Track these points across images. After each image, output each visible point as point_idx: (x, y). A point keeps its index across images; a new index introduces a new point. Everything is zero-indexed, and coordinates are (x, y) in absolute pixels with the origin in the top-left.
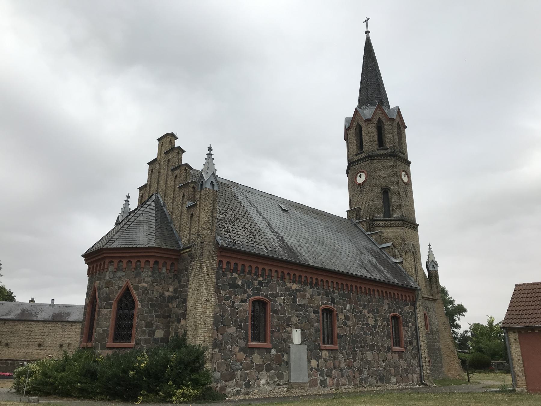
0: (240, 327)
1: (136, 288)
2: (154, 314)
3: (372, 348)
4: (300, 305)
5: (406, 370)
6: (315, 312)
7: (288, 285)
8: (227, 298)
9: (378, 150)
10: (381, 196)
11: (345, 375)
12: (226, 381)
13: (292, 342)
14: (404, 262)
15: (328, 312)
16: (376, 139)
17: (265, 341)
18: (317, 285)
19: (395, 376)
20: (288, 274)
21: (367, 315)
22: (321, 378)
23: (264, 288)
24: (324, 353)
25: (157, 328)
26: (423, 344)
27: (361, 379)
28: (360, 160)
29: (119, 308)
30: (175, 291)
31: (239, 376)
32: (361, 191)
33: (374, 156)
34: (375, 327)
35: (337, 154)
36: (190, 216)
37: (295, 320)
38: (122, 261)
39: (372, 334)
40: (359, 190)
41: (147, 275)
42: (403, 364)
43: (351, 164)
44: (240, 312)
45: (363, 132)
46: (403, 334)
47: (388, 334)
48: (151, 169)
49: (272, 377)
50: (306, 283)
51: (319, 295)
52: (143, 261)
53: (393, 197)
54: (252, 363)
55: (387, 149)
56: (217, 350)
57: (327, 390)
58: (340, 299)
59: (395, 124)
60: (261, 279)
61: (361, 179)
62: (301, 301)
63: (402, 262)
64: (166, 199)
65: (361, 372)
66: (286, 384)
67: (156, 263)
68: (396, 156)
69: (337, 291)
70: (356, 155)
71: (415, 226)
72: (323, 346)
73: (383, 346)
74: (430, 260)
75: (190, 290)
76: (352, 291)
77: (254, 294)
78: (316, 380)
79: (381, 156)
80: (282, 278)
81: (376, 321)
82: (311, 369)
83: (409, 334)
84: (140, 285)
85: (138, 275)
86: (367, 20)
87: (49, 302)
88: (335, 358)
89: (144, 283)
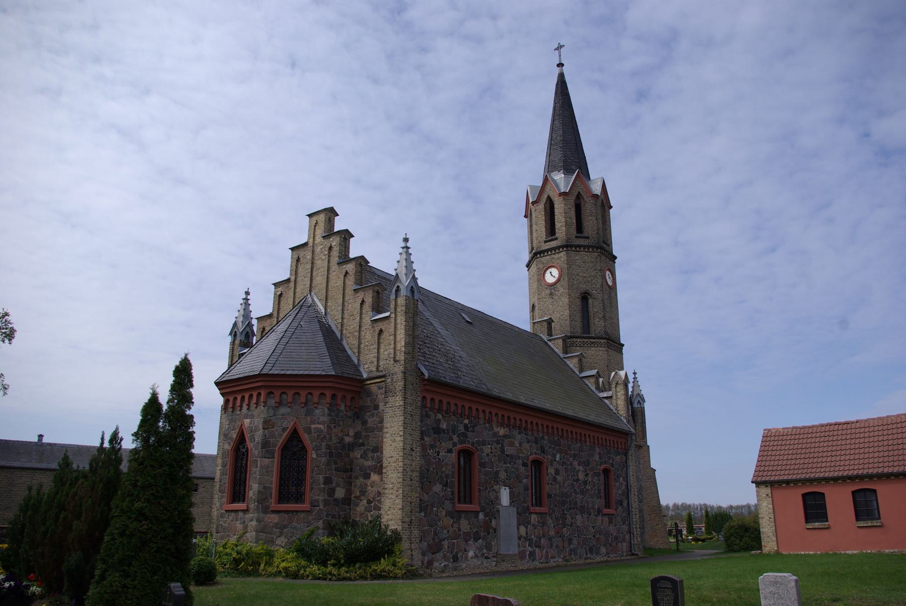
0: (446, 485)
1: (308, 430)
2: (333, 466)
3: (582, 510)
4: (507, 456)
5: (616, 538)
6: (525, 465)
7: (496, 429)
8: (432, 446)
9: (577, 237)
10: (578, 302)
11: (554, 545)
12: (433, 554)
13: (500, 504)
14: (614, 398)
15: (537, 464)
16: (574, 225)
17: (471, 503)
18: (526, 429)
19: (605, 545)
20: (496, 414)
21: (577, 467)
22: (530, 549)
23: (470, 434)
24: (533, 516)
25: (338, 485)
26: (635, 504)
27: (571, 550)
28: (550, 250)
29: (283, 457)
30: (357, 435)
31: (446, 547)
32: (551, 294)
33: (571, 246)
34: (585, 483)
35: (515, 237)
36: (377, 332)
37: (503, 475)
38: (272, 393)
39: (582, 492)
40: (548, 292)
41: (321, 413)
42: (612, 529)
43: (536, 255)
44: (446, 464)
45: (556, 211)
46: (614, 491)
47: (599, 491)
48: (296, 257)
49: (480, 549)
50: (514, 427)
51: (528, 442)
52: (316, 393)
53: (595, 306)
54: (459, 530)
55: (588, 238)
56: (423, 514)
57: (536, 564)
58: (550, 447)
59: (599, 202)
60: (466, 421)
61: (552, 276)
62: (509, 450)
63: (611, 397)
64: (329, 304)
65: (570, 541)
66: (494, 557)
67: (334, 396)
68: (601, 248)
69: (546, 437)
70: (545, 242)
71: (618, 346)
72: (532, 509)
73: (593, 508)
74: (635, 393)
75: (388, 435)
76: (562, 436)
77: (461, 442)
78: (524, 552)
79: (580, 246)
80: (490, 421)
81: (587, 475)
82: (519, 538)
83: (620, 492)
84: (313, 426)
85: (309, 413)
86: (560, 47)
87: (36, 440)
88: (544, 524)
89: (317, 422)
